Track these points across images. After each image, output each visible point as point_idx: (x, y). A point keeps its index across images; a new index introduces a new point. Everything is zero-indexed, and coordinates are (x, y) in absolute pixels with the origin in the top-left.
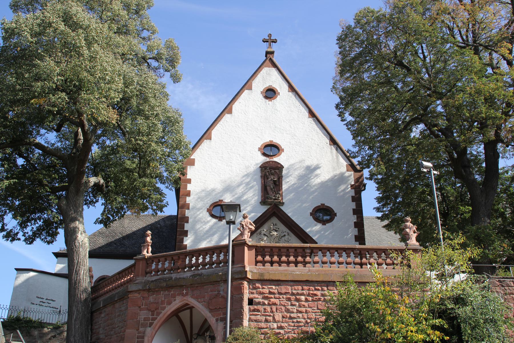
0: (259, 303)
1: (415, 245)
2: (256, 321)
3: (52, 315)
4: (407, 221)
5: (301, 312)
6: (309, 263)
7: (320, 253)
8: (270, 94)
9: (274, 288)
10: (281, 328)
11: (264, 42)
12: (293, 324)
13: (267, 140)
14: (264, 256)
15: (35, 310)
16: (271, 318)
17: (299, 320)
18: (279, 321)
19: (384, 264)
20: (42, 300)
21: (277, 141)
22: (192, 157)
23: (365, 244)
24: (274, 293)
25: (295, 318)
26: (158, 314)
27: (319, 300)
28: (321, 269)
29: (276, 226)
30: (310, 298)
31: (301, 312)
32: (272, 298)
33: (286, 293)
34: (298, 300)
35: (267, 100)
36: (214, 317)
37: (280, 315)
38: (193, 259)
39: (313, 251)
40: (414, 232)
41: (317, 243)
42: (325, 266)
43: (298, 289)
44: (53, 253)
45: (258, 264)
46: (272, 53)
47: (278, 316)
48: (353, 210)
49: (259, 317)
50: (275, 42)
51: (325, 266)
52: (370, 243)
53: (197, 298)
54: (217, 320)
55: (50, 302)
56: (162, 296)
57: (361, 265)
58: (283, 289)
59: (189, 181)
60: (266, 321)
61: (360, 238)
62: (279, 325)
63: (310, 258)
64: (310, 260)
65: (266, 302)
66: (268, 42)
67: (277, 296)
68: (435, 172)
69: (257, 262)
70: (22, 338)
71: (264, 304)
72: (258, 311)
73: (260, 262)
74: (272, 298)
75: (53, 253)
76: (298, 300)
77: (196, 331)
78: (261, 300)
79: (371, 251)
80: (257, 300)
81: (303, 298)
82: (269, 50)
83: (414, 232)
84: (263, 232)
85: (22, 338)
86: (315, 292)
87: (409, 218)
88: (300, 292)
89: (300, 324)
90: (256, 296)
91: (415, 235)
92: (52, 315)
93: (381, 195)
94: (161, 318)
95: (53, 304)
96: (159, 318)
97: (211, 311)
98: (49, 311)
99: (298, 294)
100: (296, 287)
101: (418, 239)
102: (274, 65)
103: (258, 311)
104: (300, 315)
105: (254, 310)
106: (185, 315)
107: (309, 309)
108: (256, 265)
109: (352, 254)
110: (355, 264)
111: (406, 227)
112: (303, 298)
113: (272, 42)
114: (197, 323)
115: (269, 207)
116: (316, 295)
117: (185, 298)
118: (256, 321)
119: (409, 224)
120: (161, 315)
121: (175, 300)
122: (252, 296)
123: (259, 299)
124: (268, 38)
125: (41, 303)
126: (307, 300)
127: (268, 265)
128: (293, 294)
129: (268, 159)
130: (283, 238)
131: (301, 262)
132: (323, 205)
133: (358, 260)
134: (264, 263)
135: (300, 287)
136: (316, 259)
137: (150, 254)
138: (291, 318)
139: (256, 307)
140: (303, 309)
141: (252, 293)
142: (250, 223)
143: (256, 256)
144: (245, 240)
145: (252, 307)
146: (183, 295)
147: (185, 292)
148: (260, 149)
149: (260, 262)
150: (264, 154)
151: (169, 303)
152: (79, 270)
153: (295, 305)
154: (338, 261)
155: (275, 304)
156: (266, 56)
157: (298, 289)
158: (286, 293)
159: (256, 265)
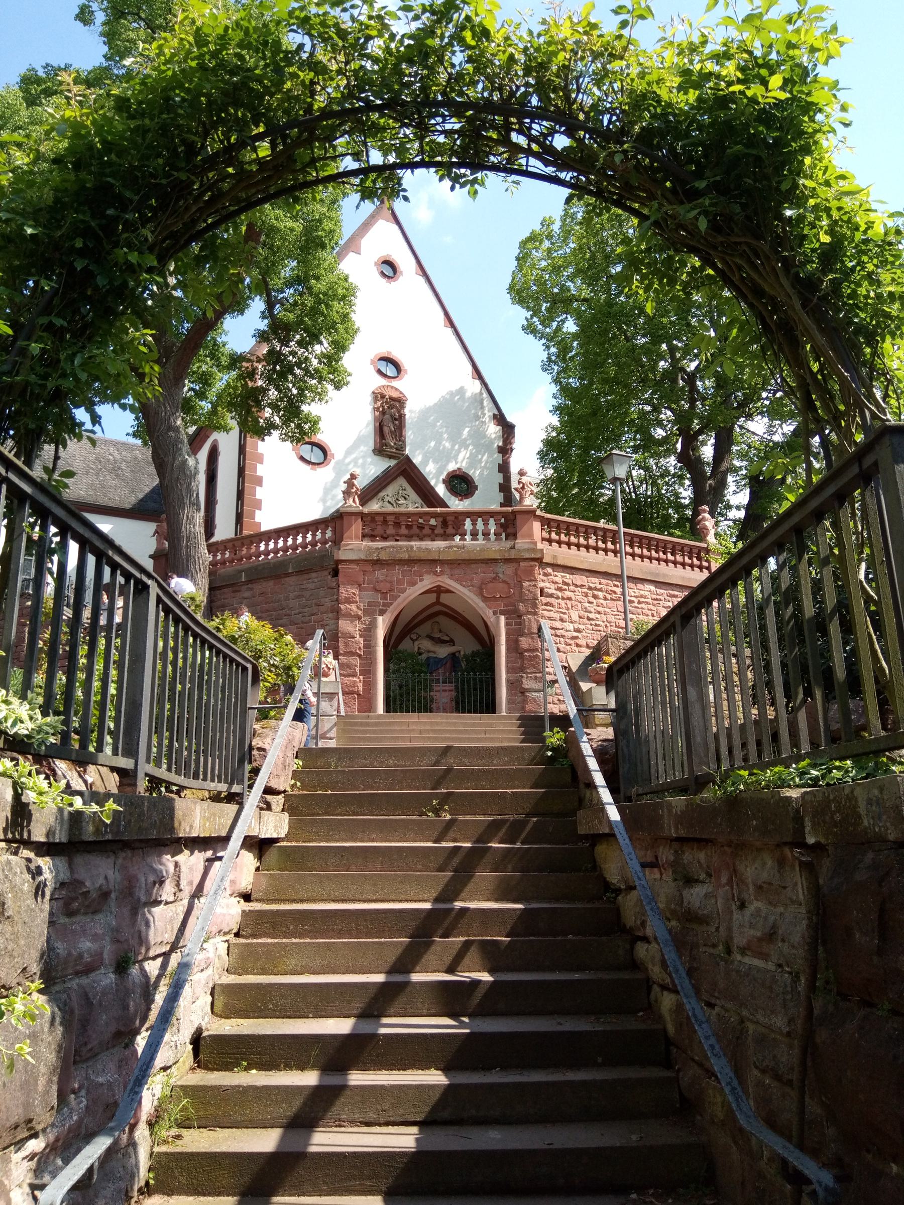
0: (551, 596)
4: (704, 511)
5: (599, 613)
8: (388, 271)
9: (568, 578)
16: (566, 617)
26: (395, 598)
30: (609, 597)
31: (599, 613)
33: (582, 586)
34: (595, 597)
36: (490, 608)
47: (575, 616)
48: (261, 485)
49: (552, 614)
53: (459, 581)
54: (495, 613)
56: (397, 573)
58: (580, 579)
60: (562, 620)
65: (560, 594)
67: (572, 588)
72: (551, 605)
76: (595, 597)
80: (550, 591)
81: (601, 594)
84: (387, 499)
86: (615, 589)
87: (706, 508)
88: (599, 586)
90: (547, 585)
93: (550, 472)
94: (399, 605)
96: (395, 604)
97: (485, 599)
99: (596, 589)
100: (593, 579)
103: (551, 605)
104: (598, 616)
111: (704, 519)
112: (601, 594)
115: (393, 463)
116: (615, 593)
117: (439, 579)
120: (399, 600)
121: (421, 580)
126: (605, 599)
128: (590, 588)
129: (383, 382)
135: (597, 580)
138: (589, 619)
139: (548, 600)
146: (435, 573)
147: (438, 569)
151: (414, 584)
155: (570, 599)
157: (594, 581)
158: (582, 586)
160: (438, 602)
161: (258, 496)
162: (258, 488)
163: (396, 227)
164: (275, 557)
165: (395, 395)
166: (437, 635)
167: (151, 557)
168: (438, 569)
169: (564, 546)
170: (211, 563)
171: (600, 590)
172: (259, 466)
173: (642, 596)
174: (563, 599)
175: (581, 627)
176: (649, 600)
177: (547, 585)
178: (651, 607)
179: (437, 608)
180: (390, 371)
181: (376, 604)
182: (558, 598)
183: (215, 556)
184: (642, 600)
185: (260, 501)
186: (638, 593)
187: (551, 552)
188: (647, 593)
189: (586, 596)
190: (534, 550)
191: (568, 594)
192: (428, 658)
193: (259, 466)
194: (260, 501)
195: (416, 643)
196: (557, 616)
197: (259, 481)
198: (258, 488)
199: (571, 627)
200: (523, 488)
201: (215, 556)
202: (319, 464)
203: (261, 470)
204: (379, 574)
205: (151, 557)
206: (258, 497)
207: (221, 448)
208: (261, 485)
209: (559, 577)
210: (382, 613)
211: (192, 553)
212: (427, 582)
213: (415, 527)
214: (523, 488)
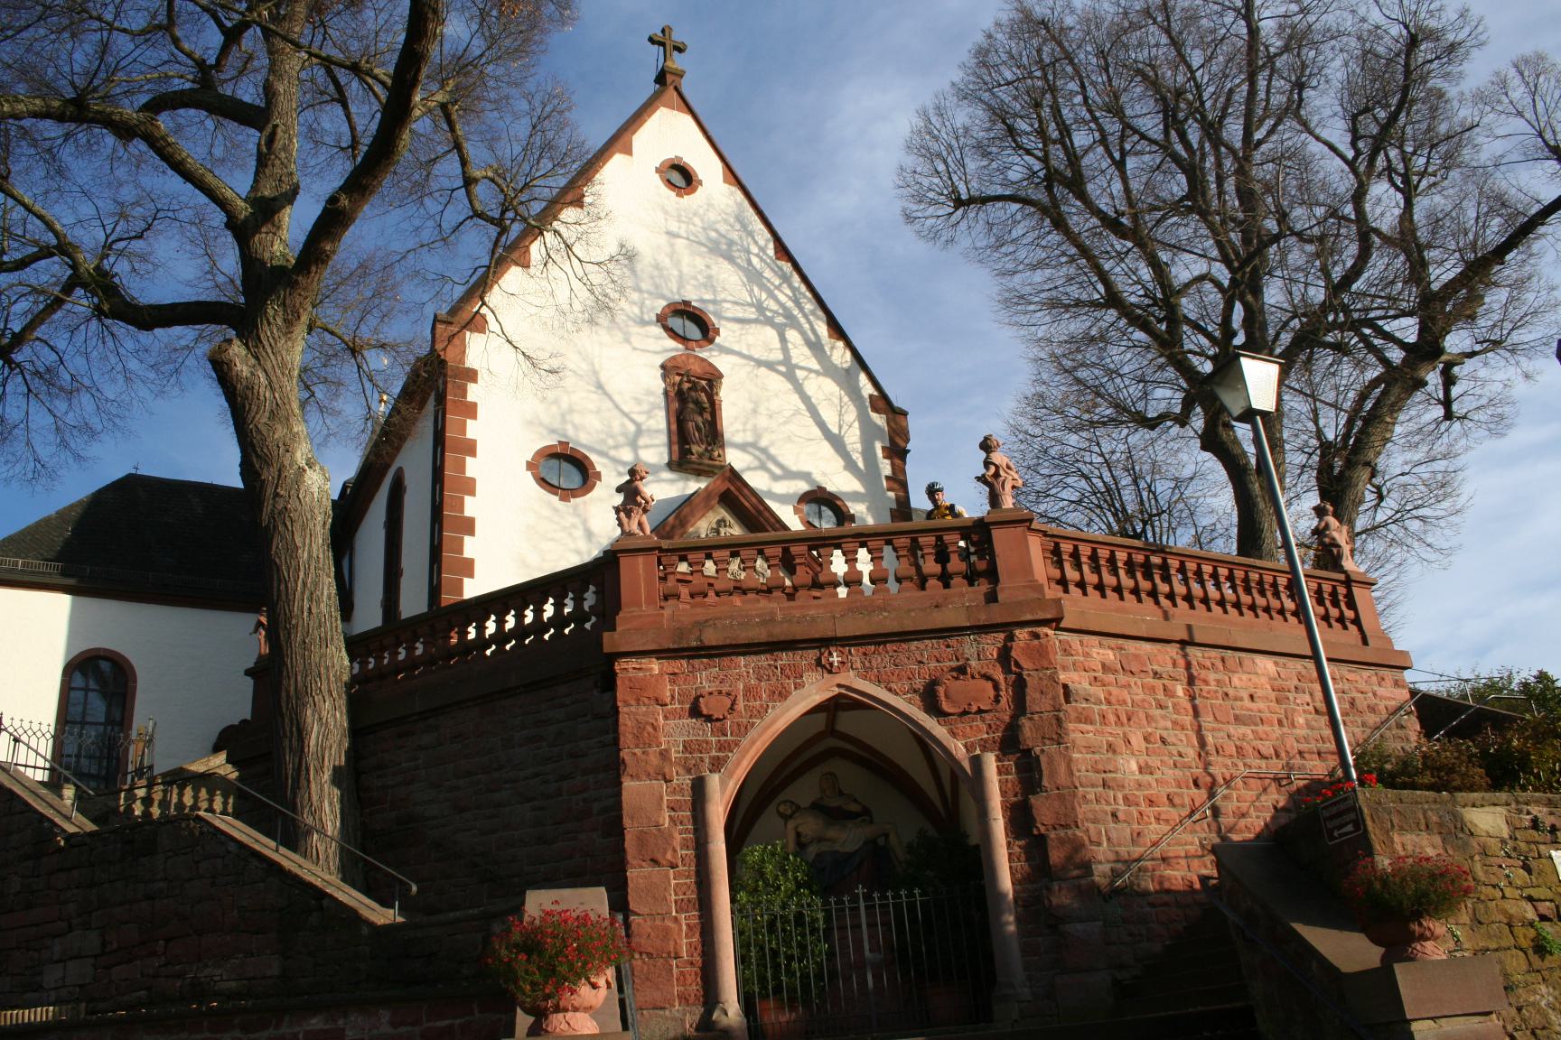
8: (676, 178)
26: (743, 729)
48: (472, 533)
147: (835, 659)
151: (783, 695)
152: (316, 584)
160: (831, 730)
161: (469, 511)
162: (467, 539)
163: (688, 119)
164: (559, 635)
166: (834, 803)
167: (248, 673)
168: (835, 659)
170: (354, 680)
172: (468, 499)
179: (833, 742)
180: (693, 331)
181: (702, 746)
183: (364, 664)
185: (474, 405)
190: (1041, 602)
192: (819, 855)
193: (468, 499)
194: (474, 405)
195: (791, 824)
197: (469, 526)
198: (467, 539)
200: (997, 475)
201: (364, 664)
203: (471, 507)
204: (705, 678)
205: (248, 673)
206: (468, 513)
207: (409, 481)
208: (472, 533)
211: (315, 658)
212: (813, 691)
213: (711, 594)
214: (997, 475)
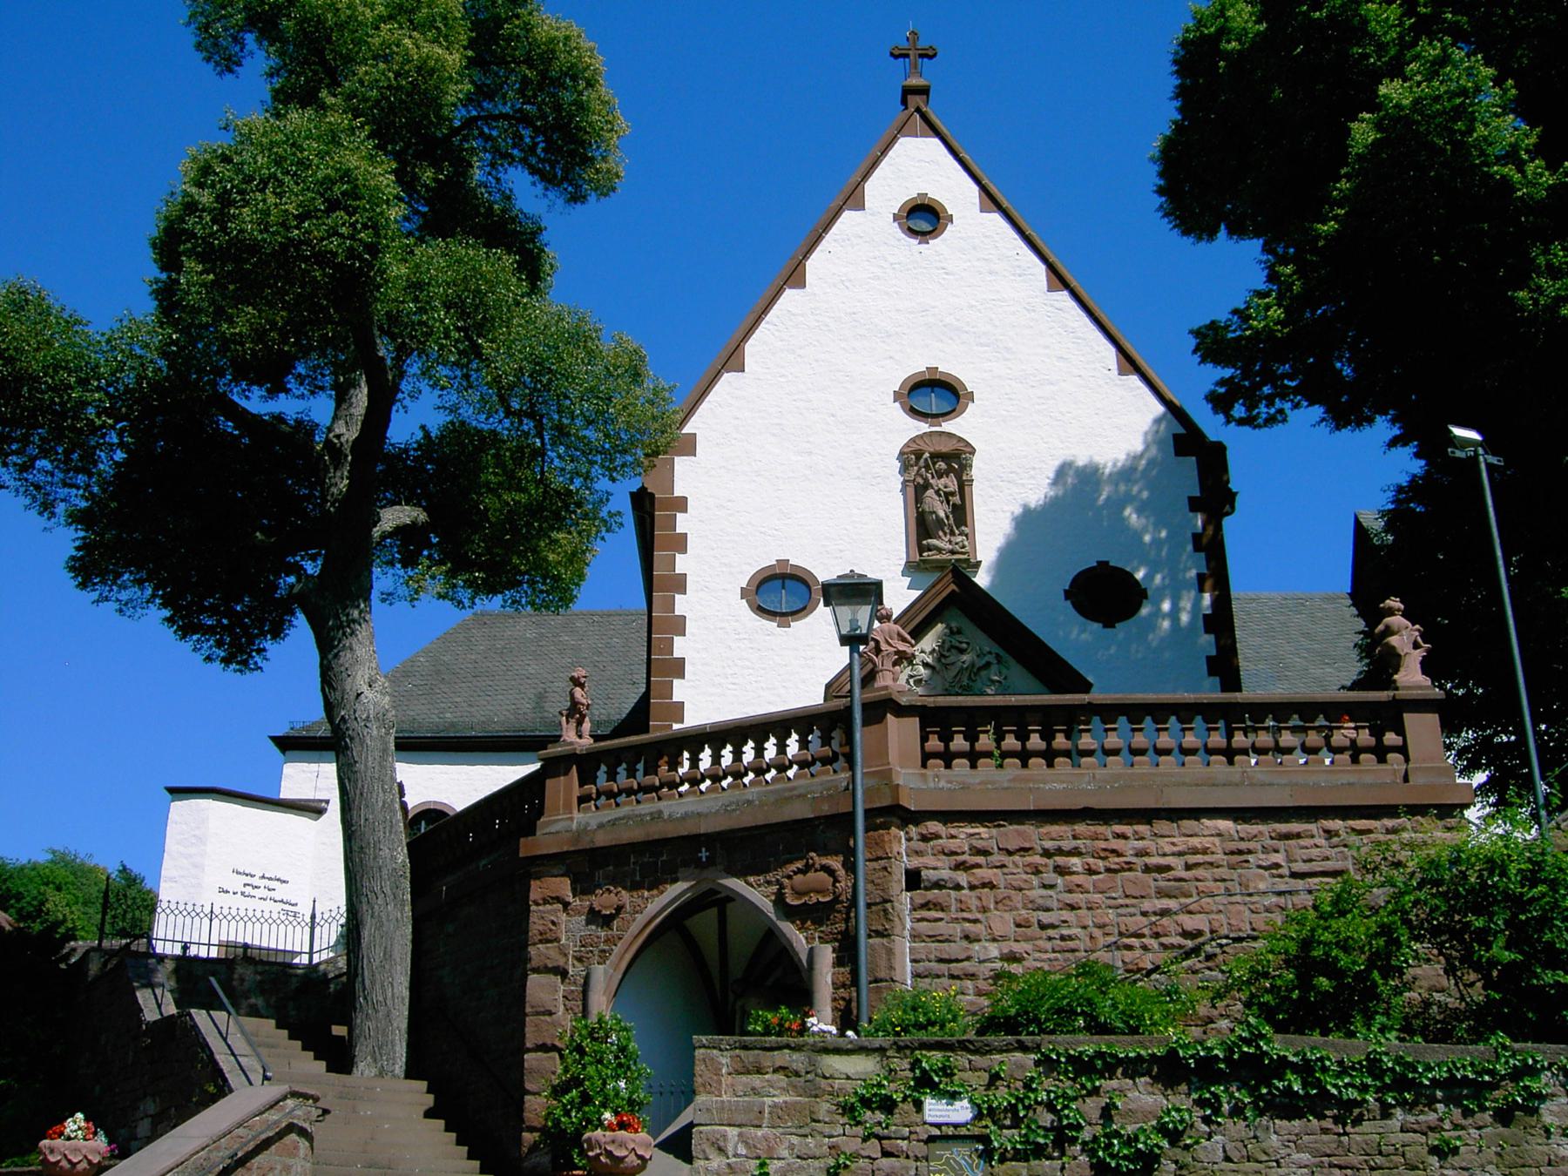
0: (938, 885)
1: (1420, 688)
2: (933, 938)
3: (282, 927)
4: (1391, 612)
5: (1072, 907)
6: (1090, 753)
7: (1123, 719)
10: (1012, 958)
11: (896, 57)
12: (1048, 945)
13: (917, 365)
14: (946, 738)
15: (259, 915)
17: (1065, 932)
18: (1004, 938)
19: (1298, 750)
20: (248, 880)
21: (949, 366)
22: (687, 430)
23: (1240, 690)
24: (985, 853)
25: (1053, 926)
27: (1129, 867)
28: (1154, 770)
29: (958, 637)
31: (1072, 907)
32: (978, 866)
34: (1061, 871)
35: (915, 242)
37: (1009, 917)
38: (724, 752)
39: (1072, 719)
40: (1416, 646)
41: (1086, 687)
42: (1141, 763)
43: (1061, 838)
44: (274, 739)
45: (931, 762)
46: (924, 91)
47: (1002, 922)
50: (931, 57)
51: (1141, 763)
52: (1254, 689)
55: (273, 884)
57: (1230, 754)
58: (1012, 834)
59: (681, 504)
61: (1224, 666)
62: (1006, 951)
63: (1068, 737)
64: (1094, 745)
65: (962, 878)
66: (907, 56)
67: (997, 858)
68: (1493, 460)
69: (926, 757)
70: (225, 1000)
71: (958, 887)
73: (935, 755)
74: (978, 866)
75: (274, 739)
76: (1061, 871)
77: (737, 969)
78: (945, 874)
79: (1259, 711)
81: (1075, 862)
82: (914, 81)
83: (1416, 646)
85: (225, 1000)
87: (1394, 603)
88: (1067, 845)
89: (1071, 944)
91: (1418, 655)
92: (282, 927)
95: (281, 892)
98: (275, 916)
99: (1060, 852)
101: (1427, 667)
102: (937, 133)
104: (1066, 915)
105: (925, 906)
106: (704, 924)
107: (1097, 897)
108: (924, 765)
109: (1198, 722)
110: (1210, 751)
113: (921, 56)
114: (742, 945)
117: (707, 873)
118: (933, 938)
119: (1397, 620)
122: (915, 862)
123: (937, 868)
124: (905, 45)
125: (248, 890)
126: (1091, 871)
127: (962, 766)
129: (923, 427)
130: (983, 673)
131: (1067, 754)
132: (1103, 565)
133: (1217, 739)
134: (948, 758)
136: (1086, 741)
137: (587, 741)
140: (1077, 898)
141: (918, 853)
142: (899, 634)
143: (924, 739)
144: (886, 688)
145: (920, 896)
147: (704, 854)
148: (897, 396)
149: (935, 755)
150: (914, 412)
153: (1052, 887)
154: (1180, 746)
155: (991, 885)
156: (904, 102)
158: (1024, 850)
159: (924, 765)
162: (676, 682)
163: (936, 141)
165: (945, 448)
169: (961, 764)
171: (1075, 852)
173: (1195, 851)
174: (972, 887)
175: (1018, 948)
176: (1219, 857)
177: (929, 860)
178: (1223, 872)
182: (958, 887)
184: (1192, 859)
186: (1182, 843)
187: (917, 783)
188: (1207, 842)
189: (1037, 872)
191: (984, 874)
196: (957, 930)
198: (676, 682)
199: (994, 950)
202: (793, 613)
208: (682, 676)
209: (962, 836)
210: (604, 956)
